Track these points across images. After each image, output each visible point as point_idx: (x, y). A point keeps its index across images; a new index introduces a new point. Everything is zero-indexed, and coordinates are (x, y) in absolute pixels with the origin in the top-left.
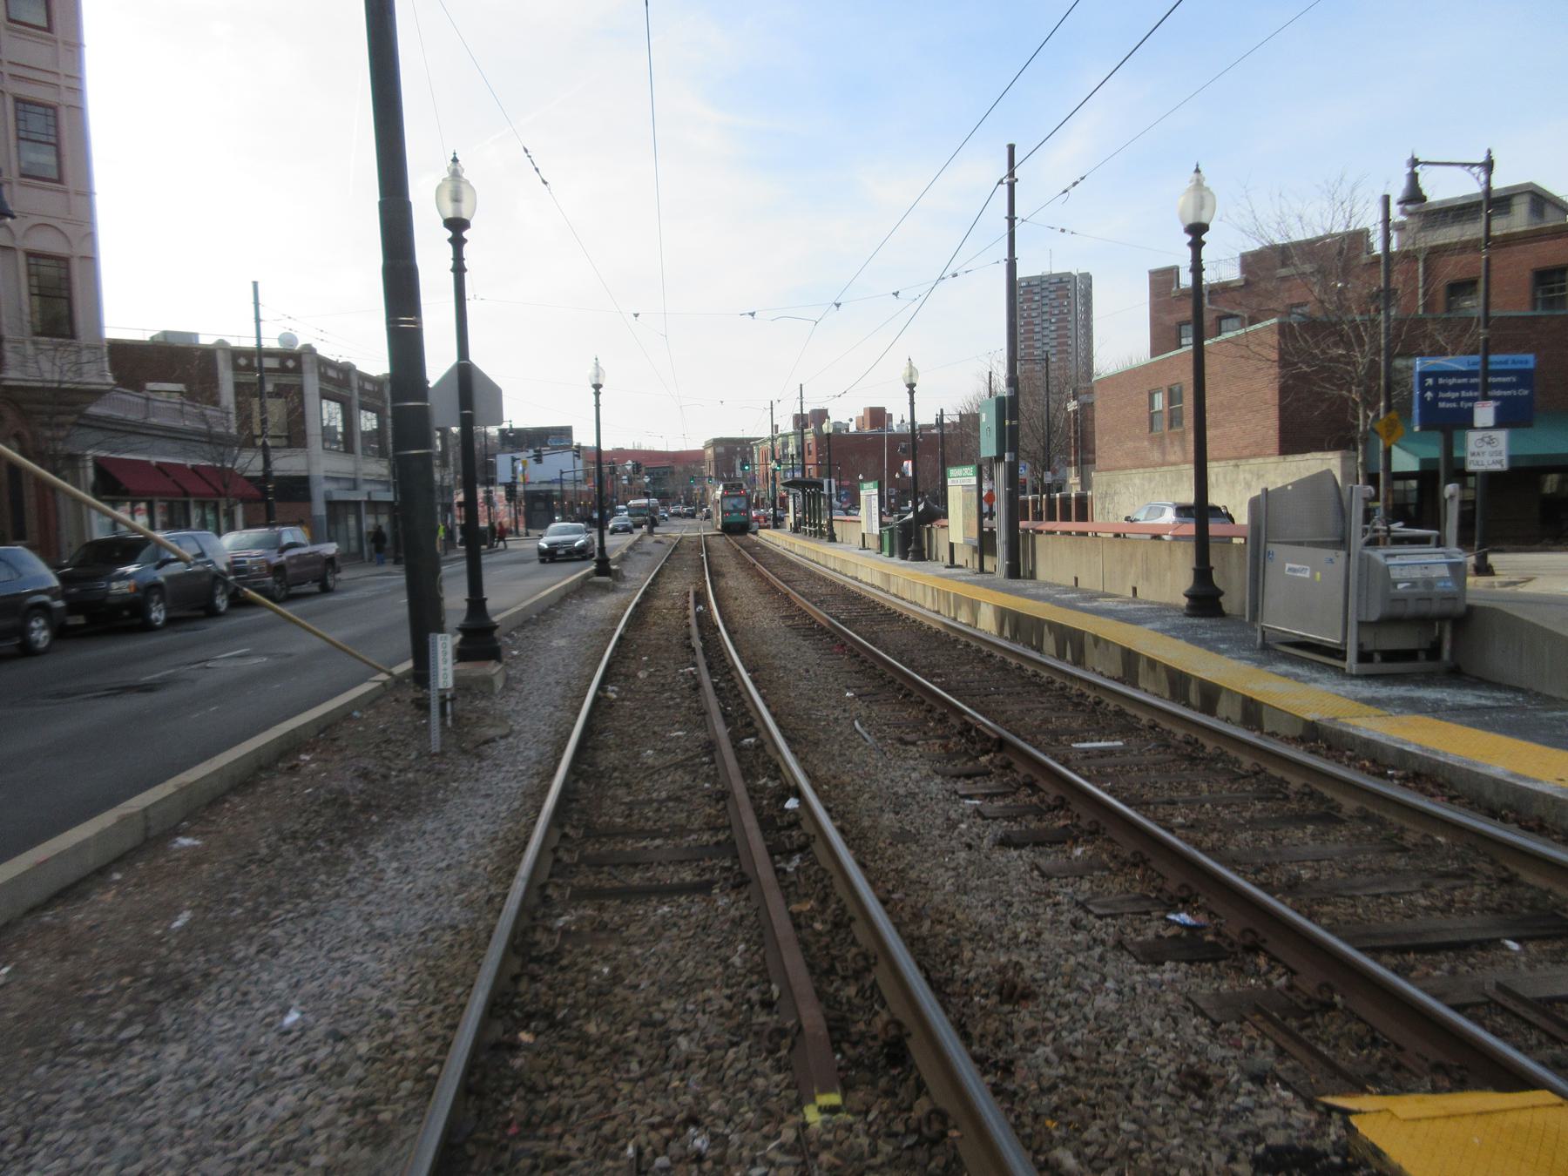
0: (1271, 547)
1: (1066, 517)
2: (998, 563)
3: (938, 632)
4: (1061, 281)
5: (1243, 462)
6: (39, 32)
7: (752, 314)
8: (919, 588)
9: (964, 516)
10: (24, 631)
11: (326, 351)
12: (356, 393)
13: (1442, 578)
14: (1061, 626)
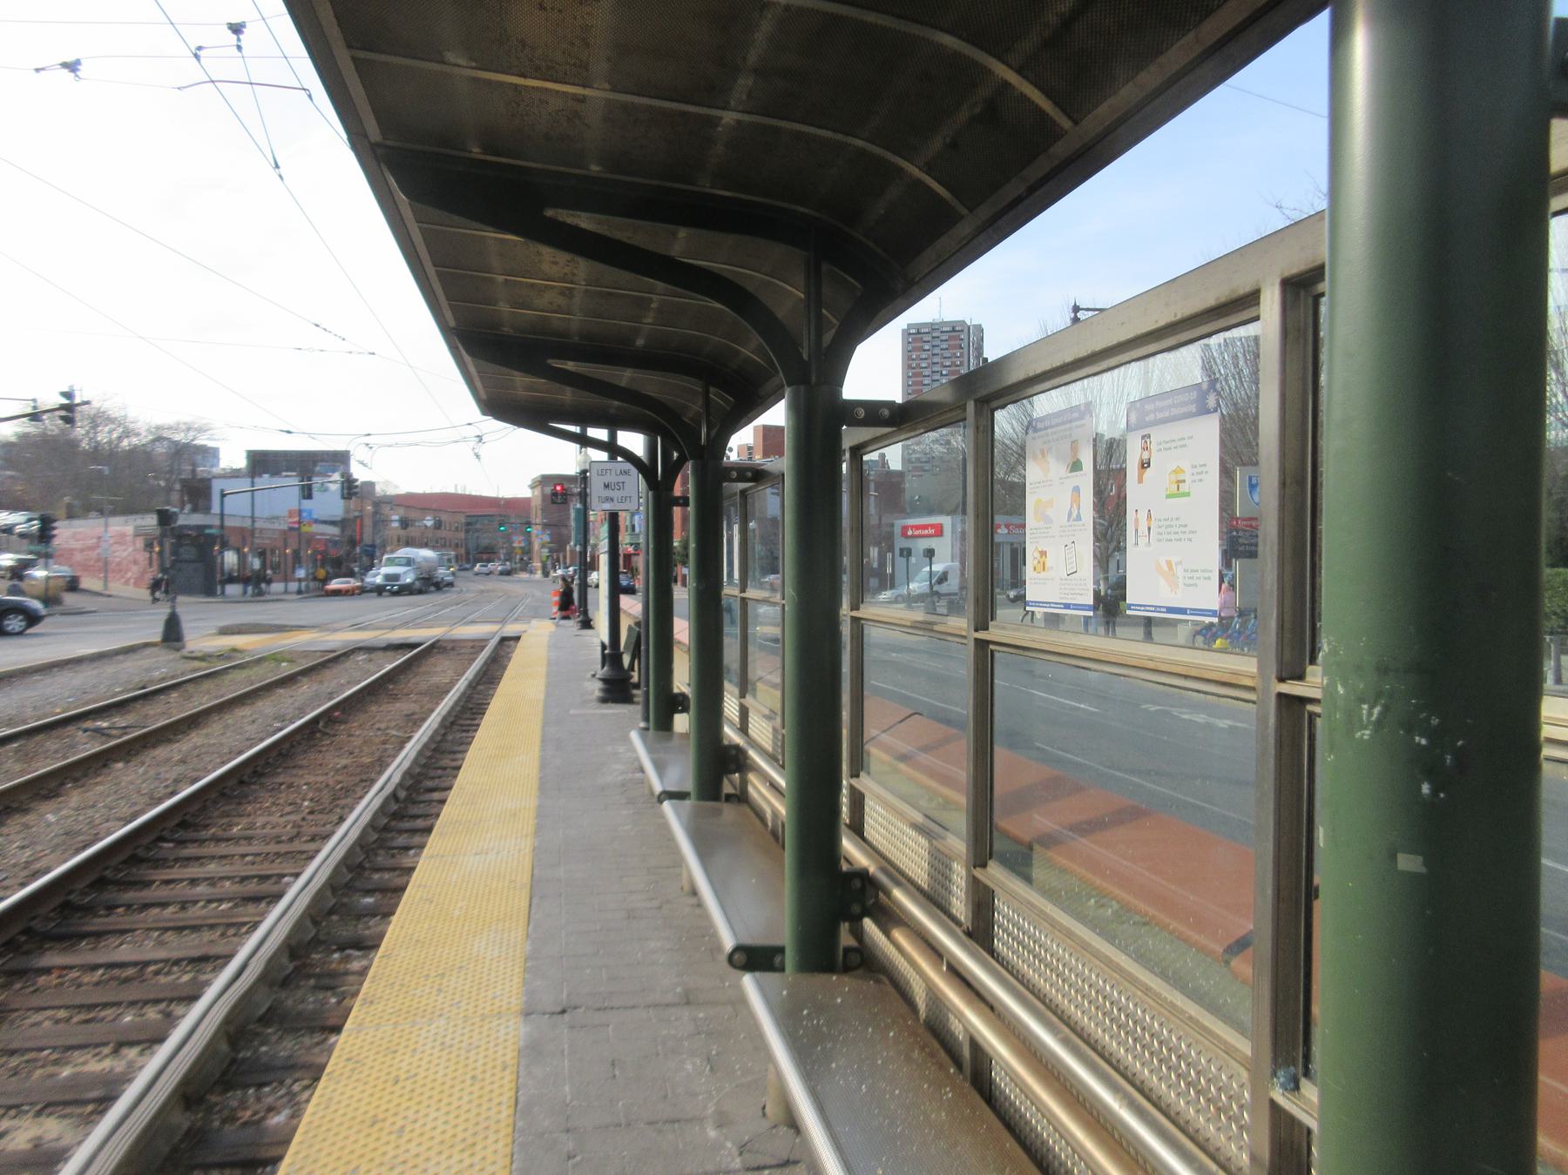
7: (72, 67)
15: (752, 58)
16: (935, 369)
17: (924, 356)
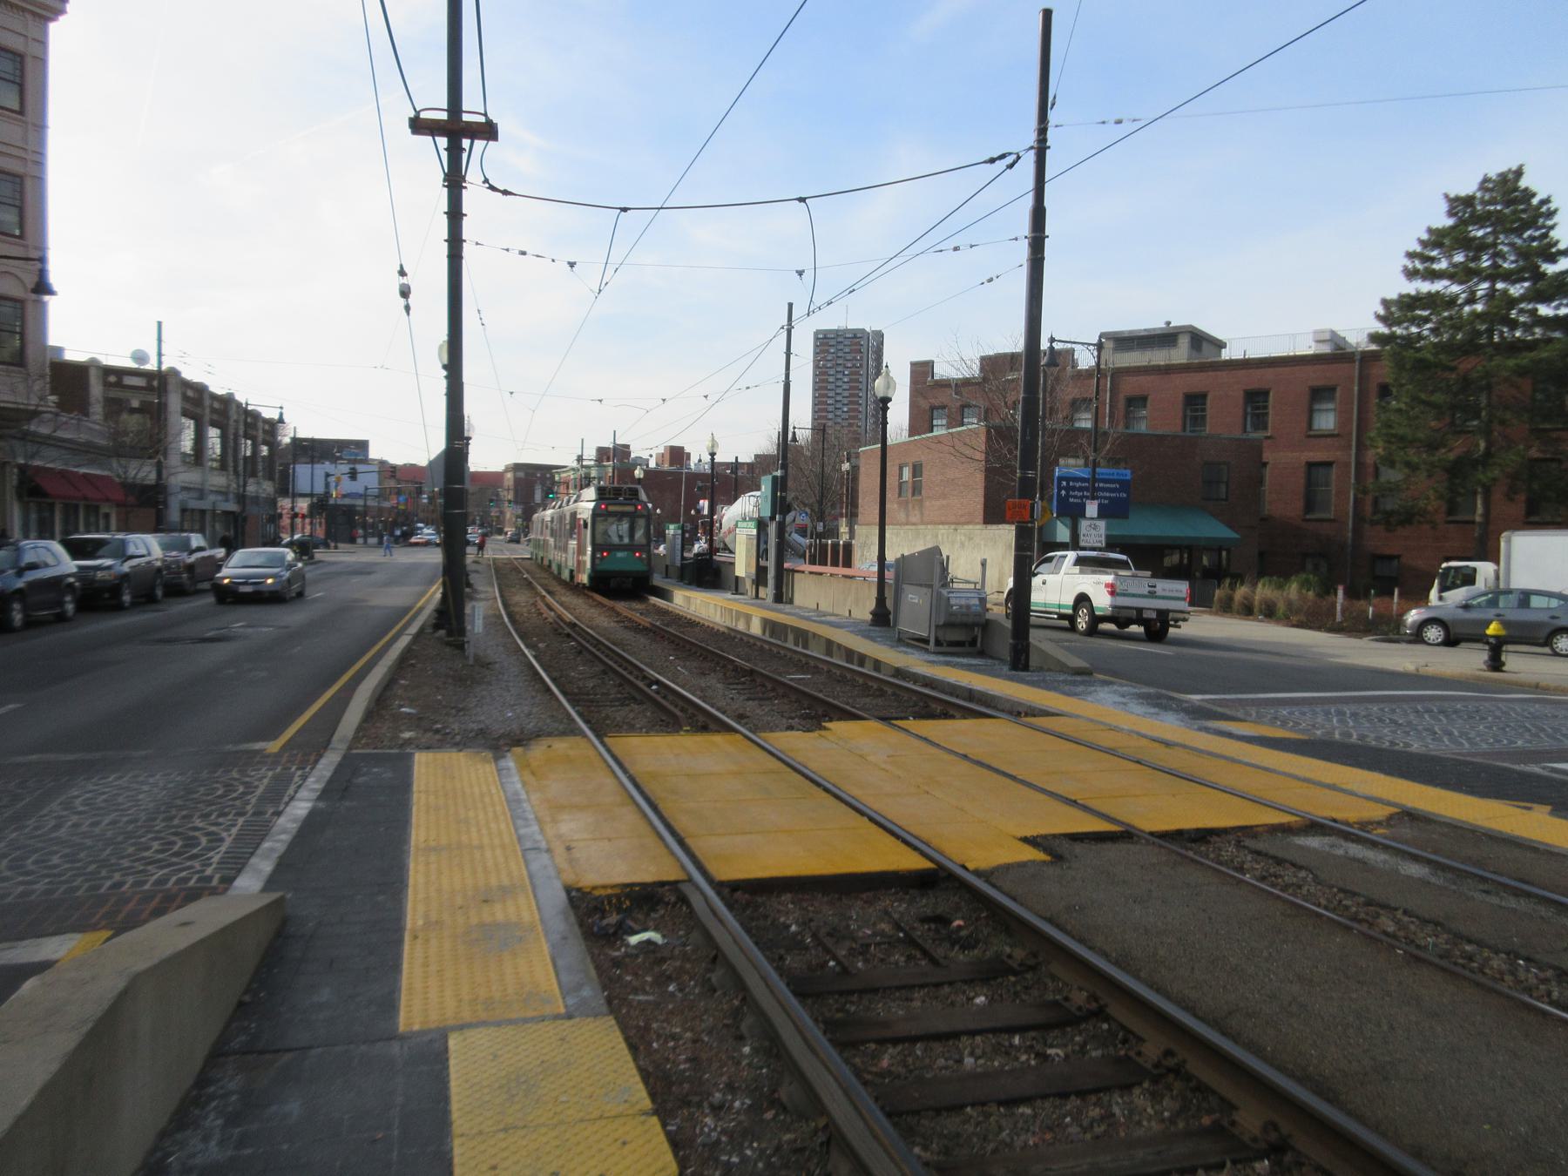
0: (904, 586)
1: (835, 564)
2: (768, 592)
3: (723, 633)
4: (855, 337)
5: (960, 527)
6: (10, 114)
7: (600, 401)
8: (712, 606)
9: (747, 557)
10: (61, 604)
11: (190, 374)
12: (207, 411)
13: (976, 605)
14: (798, 629)
15: (1357, 363)
16: (839, 369)
17: (829, 358)
